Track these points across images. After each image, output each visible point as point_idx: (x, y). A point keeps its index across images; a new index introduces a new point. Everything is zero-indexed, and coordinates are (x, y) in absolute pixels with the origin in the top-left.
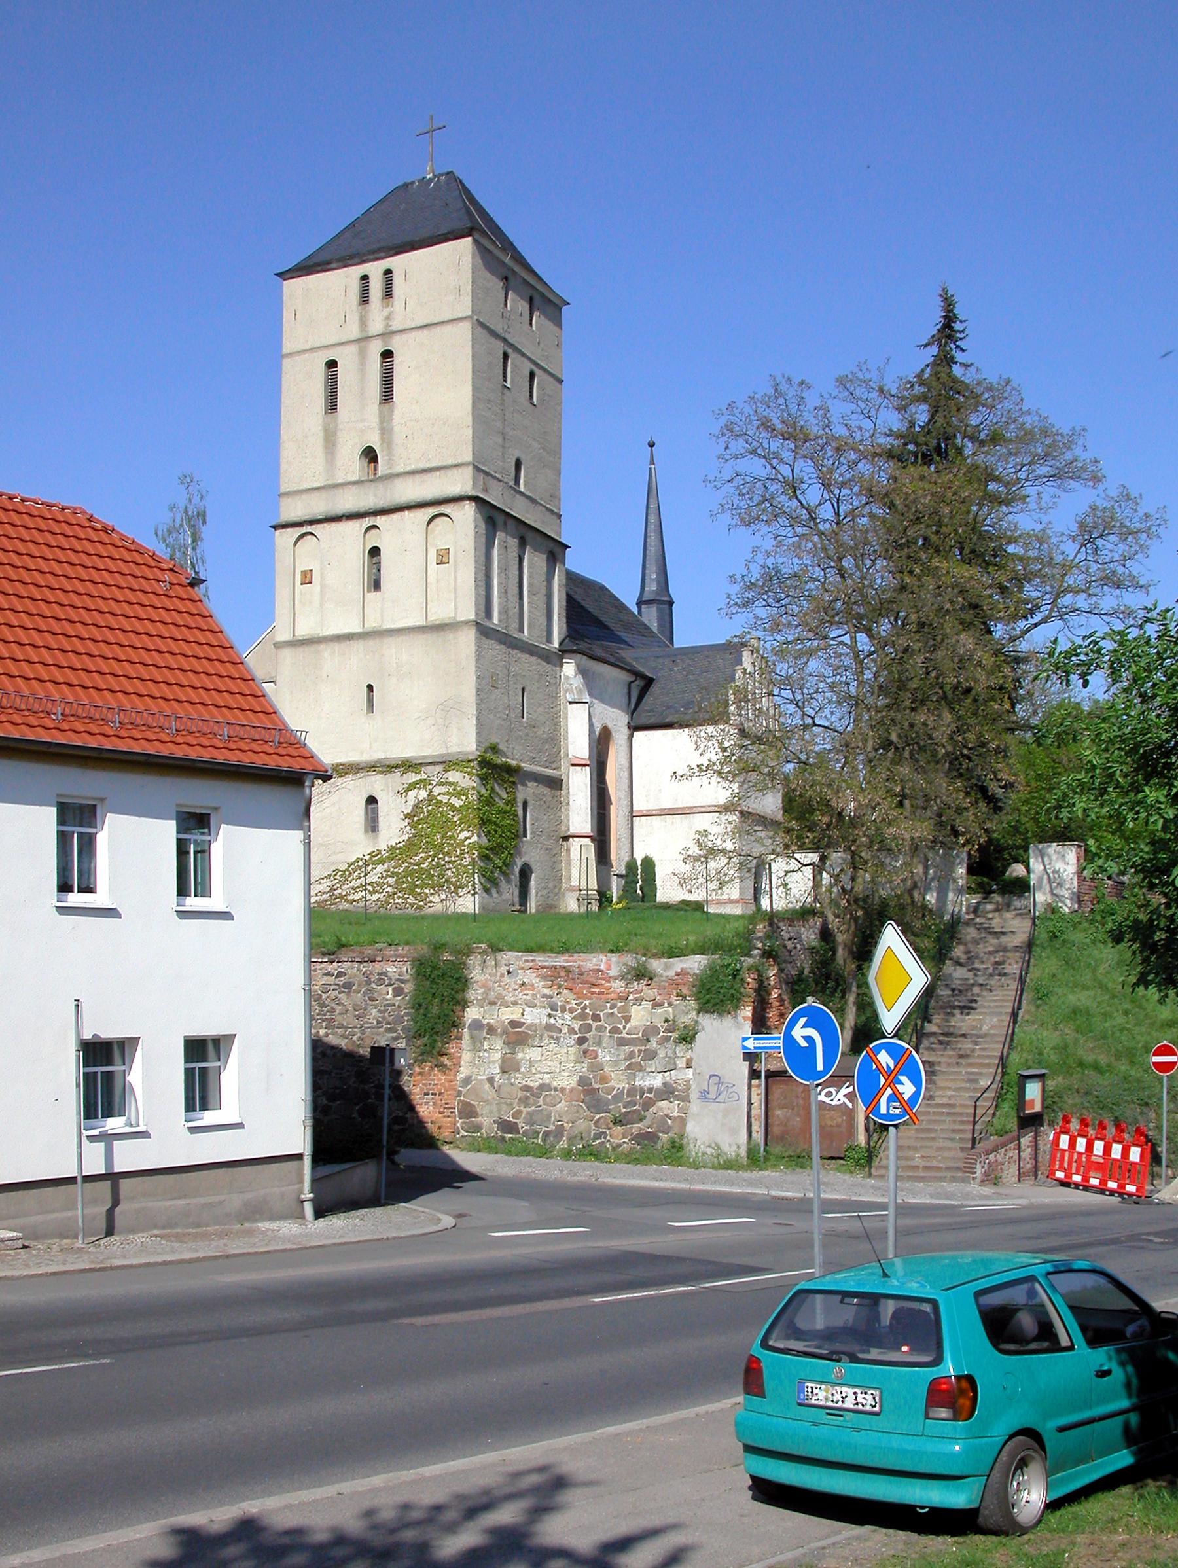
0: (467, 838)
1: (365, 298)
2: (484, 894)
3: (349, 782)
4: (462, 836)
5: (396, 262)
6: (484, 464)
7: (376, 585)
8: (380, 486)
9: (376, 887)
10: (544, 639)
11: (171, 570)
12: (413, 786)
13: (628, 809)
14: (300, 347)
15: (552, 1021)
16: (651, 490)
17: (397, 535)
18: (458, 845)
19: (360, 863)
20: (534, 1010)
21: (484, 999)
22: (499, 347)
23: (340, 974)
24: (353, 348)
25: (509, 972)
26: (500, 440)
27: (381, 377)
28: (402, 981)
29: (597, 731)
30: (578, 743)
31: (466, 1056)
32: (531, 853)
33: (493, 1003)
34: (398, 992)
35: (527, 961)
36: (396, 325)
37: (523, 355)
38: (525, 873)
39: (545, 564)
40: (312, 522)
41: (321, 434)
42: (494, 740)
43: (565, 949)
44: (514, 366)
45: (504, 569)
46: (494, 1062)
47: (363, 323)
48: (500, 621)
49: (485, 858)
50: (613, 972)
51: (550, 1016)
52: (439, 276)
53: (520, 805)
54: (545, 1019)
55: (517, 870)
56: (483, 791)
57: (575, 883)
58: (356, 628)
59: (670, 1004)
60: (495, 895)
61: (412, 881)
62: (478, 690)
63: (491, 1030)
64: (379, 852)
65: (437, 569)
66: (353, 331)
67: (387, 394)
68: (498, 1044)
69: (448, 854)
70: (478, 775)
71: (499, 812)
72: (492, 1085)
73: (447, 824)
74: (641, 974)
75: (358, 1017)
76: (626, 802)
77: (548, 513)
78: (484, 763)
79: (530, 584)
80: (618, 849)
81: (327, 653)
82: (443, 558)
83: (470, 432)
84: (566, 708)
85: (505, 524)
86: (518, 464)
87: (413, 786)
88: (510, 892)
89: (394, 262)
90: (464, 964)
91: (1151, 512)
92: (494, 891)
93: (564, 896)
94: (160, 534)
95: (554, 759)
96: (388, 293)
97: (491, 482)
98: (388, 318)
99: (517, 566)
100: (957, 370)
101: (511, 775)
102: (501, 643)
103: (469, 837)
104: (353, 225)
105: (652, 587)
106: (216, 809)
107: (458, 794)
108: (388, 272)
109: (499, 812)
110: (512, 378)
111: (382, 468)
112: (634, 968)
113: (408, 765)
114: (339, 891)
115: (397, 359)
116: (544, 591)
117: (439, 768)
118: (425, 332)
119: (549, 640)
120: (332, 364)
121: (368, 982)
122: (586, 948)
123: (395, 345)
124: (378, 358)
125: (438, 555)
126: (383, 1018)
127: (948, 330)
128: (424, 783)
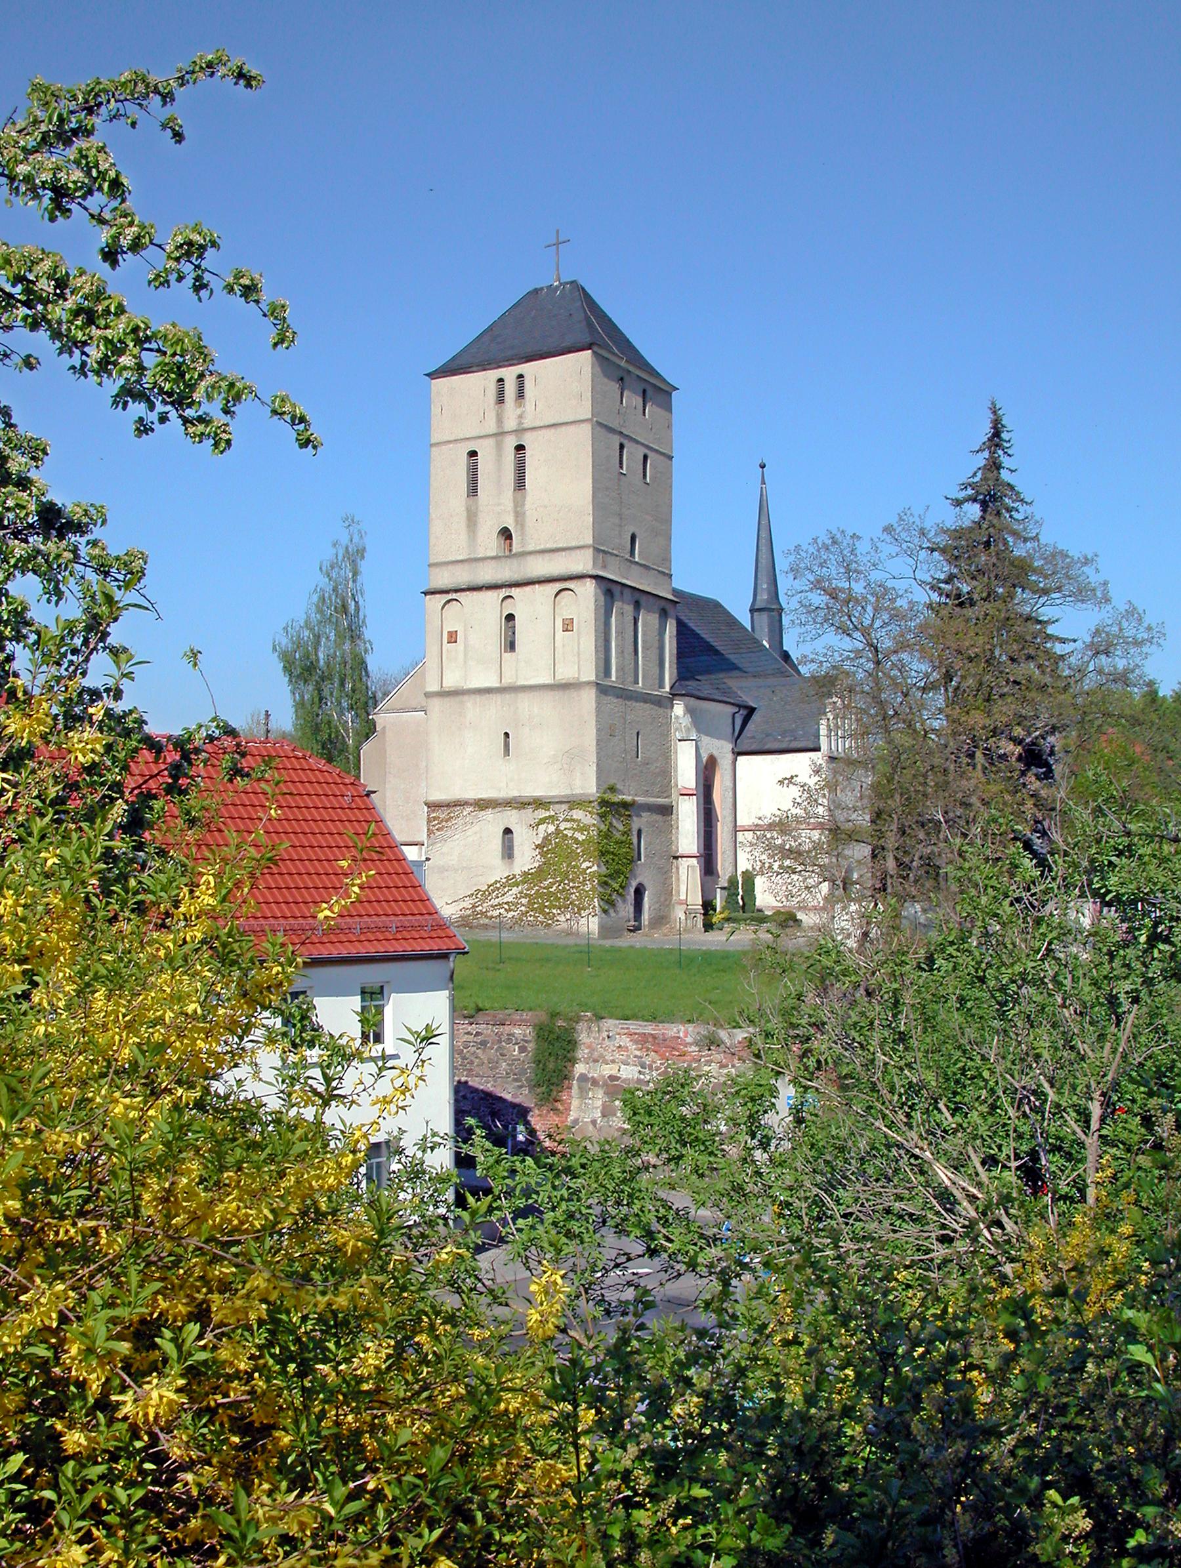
1: (500, 399)
4: (584, 866)
7: (512, 646)
8: (515, 561)
9: (511, 906)
12: (542, 821)
14: (446, 438)
22: (616, 440)
23: (478, 1034)
24: (491, 442)
26: (617, 521)
30: (686, 773)
31: (575, 1103)
32: (644, 874)
33: (595, 1061)
34: (523, 1049)
36: (527, 423)
37: (637, 442)
38: (639, 892)
40: (456, 591)
42: (612, 782)
43: (653, 1019)
47: (500, 420)
52: (564, 382)
53: (635, 833)
54: (636, 1075)
55: (632, 890)
56: (602, 827)
57: (683, 897)
58: (495, 684)
60: (613, 914)
61: (542, 903)
63: (595, 1082)
65: (562, 637)
66: (491, 427)
67: (520, 482)
68: (600, 1093)
69: (573, 880)
73: (571, 856)
74: (712, 1042)
76: (730, 818)
78: (604, 803)
80: (723, 860)
81: (470, 702)
82: (568, 626)
87: (542, 821)
89: (526, 368)
91: (1154, 625)
92: (611, 911)
95: (666, 790)
96: (521, 394)
97: (609, 558)
98: (520, 416)
100: (1005, 475)
103: (591, 867)
104: (490, 328)
105: (764, 596)
107: (581, 830)
108: (521, 376)
113: (539, 803)
116: (656, 645)
117: (565, 807)
118: (553, 430)
119: (662, 686)
120: (473, 454)
121: (500, 1041)
122: (670, 1018)
123: (527, 440)
124: (512, 451)
127: (996, 437)
128: (552, 819)
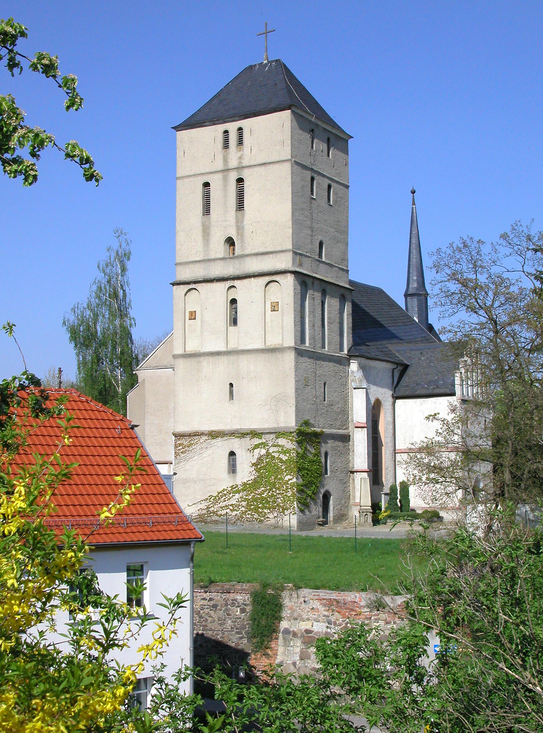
0: (289, 480)
1: (226, 145)
2: (301, 514)
3: (219, 442)
4: (287, 478)
5: (245, 123)
6: (299, 249)
7: (235, 322)
8: (237, 261)
9: (234, 507)
10: (338, 350)
11: (122, 420)
12: (257, 447)
13: (393, 449)
15: (329, 630)
16: (413, 222)
17: (246, 291)
18: (285, 484)
19: (225, 492)
20: (319, 624)
21: (291, 616)
22: (308, 175)
23: (211, 599)
24: (219, 176)
25: (305, 602)
26: (309, 232)
27: (237, 203)
28: (245, 605)
29: (372, 402)
30: (359, 412)
31: (281, 650)
32: (330, 484)
33: (296, 619)
34: (243, 611)
35: (315, 595)
36: (245, 163)
37: (324, 176)
38: (326, 497)
39: (338, 304)
40: (195, 282)
41: (201, 228)
42: (306, 418)
43: (337, 588)
44: (318, 184)
45: (312, 312)
46: (296, 653)
47: (225, 160)
48: (310, 344)
49: (300, 491)
50: (363, 603)
51: (327, 627)
52: (271, 133)
53: (323, 455)
55: (321, 496)
57: (357, 501)
58: (223, 349)
59: (395, 623)
60: (307, 513)
61: (257, 505)
62: (297, 389)
63: (295, 635)
64: (237, 486)
65: (271, 315)
66: (219, 165)
67: (240, 205)
69: (278, 489)
70: (296, 441)
71: (310, 462)
72: (295, 667)
73: (278, 471)
74: (379, 606)
75: (221, 625)
76: (391, 444)
77: (340, 272)
79: (328, 318)
81: (205, 362)
83: (290, 231)
84: (352, 391)
85: (313, 283)
86: (321, 244)
87: (257, 447)
88: (316, 510)
90: (280, 595)
93: (351, 508)
94: (101, 267)
95: (345, 423)
96: (240, 142)
97: (305, 260)
98: (240, 158)
99: (320, 309)
101: (318, 438)
102: (310, 358)
103: (291, 479)
105: (414, 285)
106: (146, 562)
107: (284, 452)
108: (240, 129)
109: (310, 462)
110: (319, 192)
111: (238, 252)
112: (375, 602)
113: (254, 434)
114: (212, 509)
115: (246, 184)
116: (338, 320)
117: (273, 436)
118: (263, 168)
119: (341, 349)
121: (226, 605)
123: (245, 174)
125: (272, 306)
126: (235, 625)
128: (264, 445)
